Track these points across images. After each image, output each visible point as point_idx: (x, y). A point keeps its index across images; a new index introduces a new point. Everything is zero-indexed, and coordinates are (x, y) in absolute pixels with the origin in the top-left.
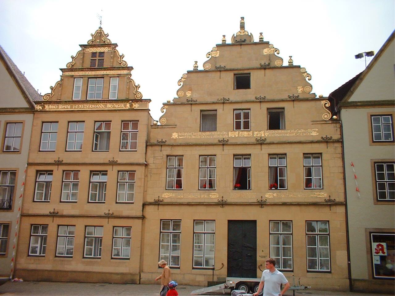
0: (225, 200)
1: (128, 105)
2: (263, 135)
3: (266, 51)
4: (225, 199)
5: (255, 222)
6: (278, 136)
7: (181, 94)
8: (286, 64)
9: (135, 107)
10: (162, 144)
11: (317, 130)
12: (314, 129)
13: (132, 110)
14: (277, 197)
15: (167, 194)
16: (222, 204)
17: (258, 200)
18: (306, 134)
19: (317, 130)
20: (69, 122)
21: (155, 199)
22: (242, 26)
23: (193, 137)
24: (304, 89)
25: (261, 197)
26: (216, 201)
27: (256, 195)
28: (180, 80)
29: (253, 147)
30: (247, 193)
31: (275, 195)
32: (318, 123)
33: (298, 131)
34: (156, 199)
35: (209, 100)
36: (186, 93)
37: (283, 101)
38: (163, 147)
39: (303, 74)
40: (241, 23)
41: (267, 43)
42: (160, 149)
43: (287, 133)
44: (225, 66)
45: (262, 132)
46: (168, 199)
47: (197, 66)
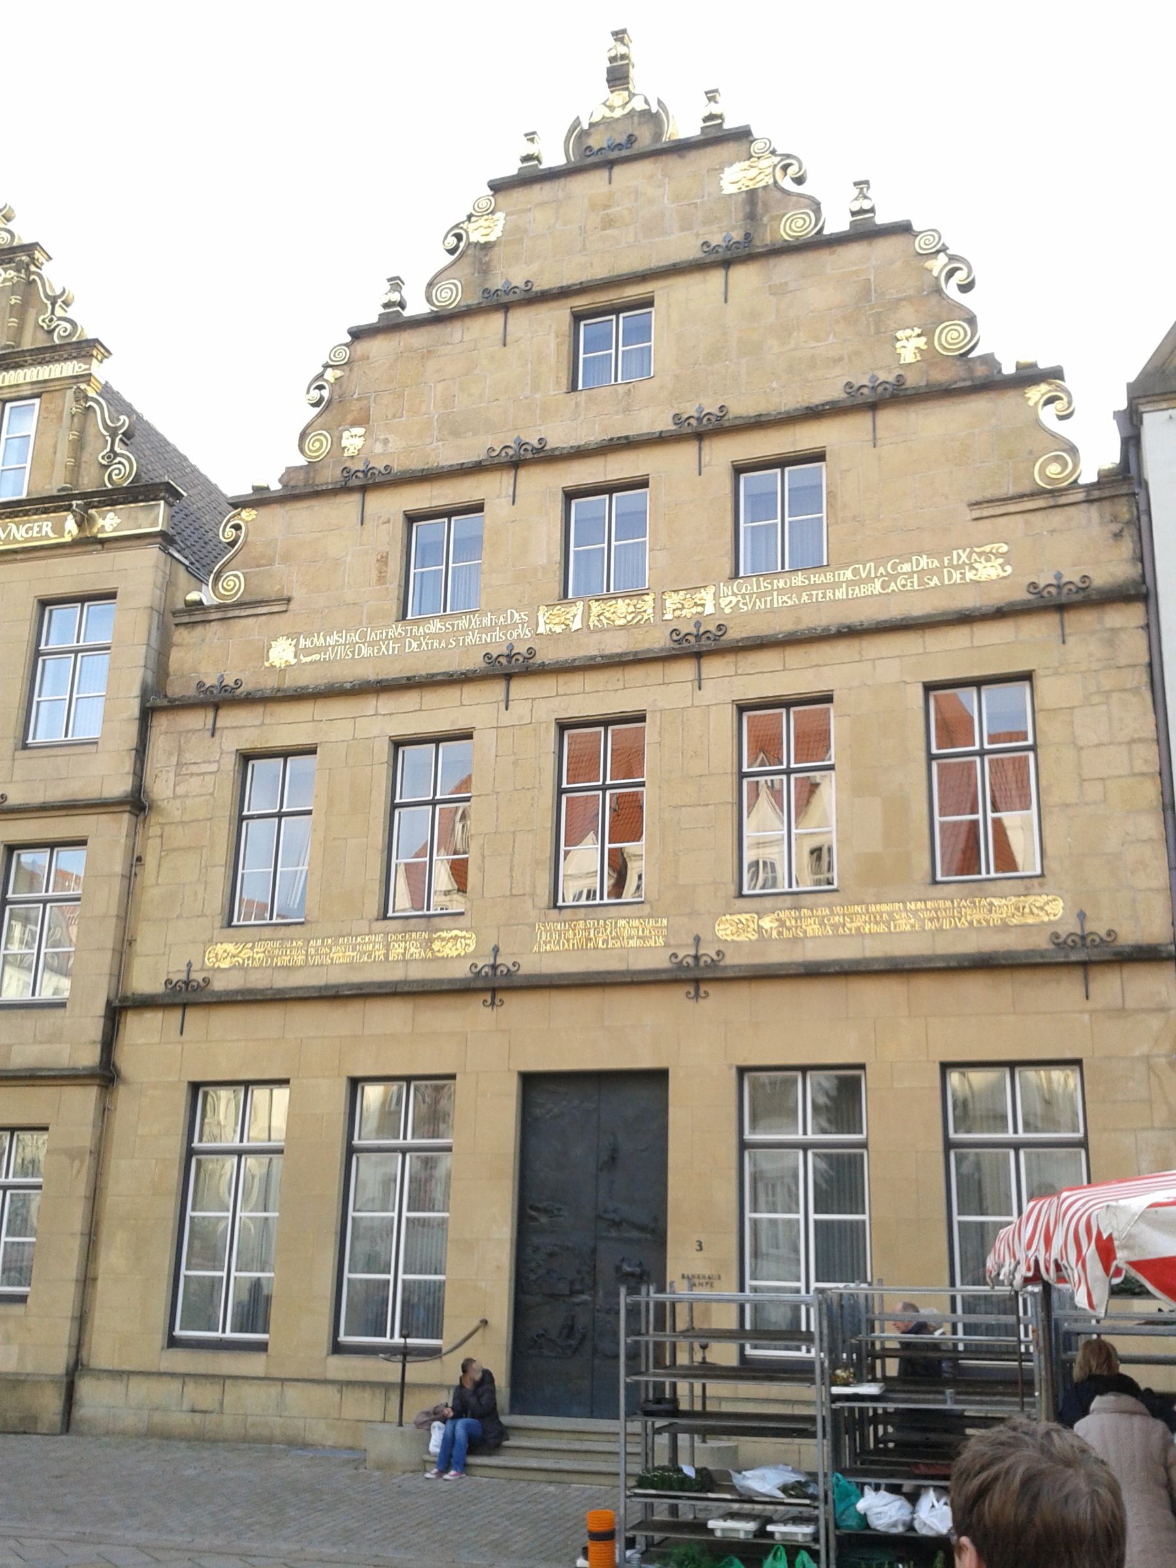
0: (510, 965)
1: (71, 526)
2: (709, 609)
3: (736, 177)
4: (505, 960)
5: (658, 1077)
6: (790, 603)
7: (955, 334)
8: (837, 222)
9: (103, 526)
10: (220, 699)
11: (1004, 548)
12: (987, 548)
13: (88, 542)
14: (780, 933)
15: (230, 948)
16: (493, 985)
17: (675, 955)
18: (941, 579)
19: (1004, 548)
20: (45, 603)
21: (171, 976)
22: (618, 76)
23: (366, 651)
24: (930, 343)
25: (691, 941)
26: (461, 971)
27: (667, 927)
28: (320, 376)
29: (655, 672)
30: (622, 922)
31: (767, 923)
32: (1012, 508)
33: (894, 568)
34: (175, 978)
35: (448, 455)
36: (341, 437)
37: (813, 414)
38: (221, 713)
39: (929, 264)
40: (612, 59)
41: (743, 135)
42: (209, 725)
43: (836, 585)
44: (527, 282)
45: (707, 596)
46: (233, 972)
47: (866, 205)
